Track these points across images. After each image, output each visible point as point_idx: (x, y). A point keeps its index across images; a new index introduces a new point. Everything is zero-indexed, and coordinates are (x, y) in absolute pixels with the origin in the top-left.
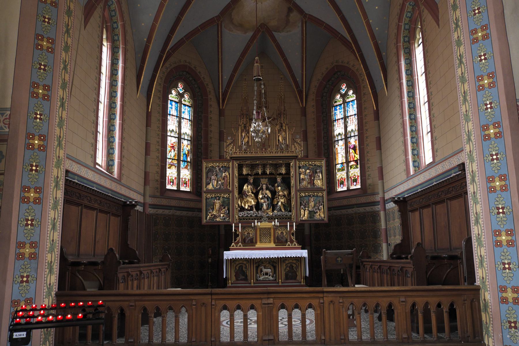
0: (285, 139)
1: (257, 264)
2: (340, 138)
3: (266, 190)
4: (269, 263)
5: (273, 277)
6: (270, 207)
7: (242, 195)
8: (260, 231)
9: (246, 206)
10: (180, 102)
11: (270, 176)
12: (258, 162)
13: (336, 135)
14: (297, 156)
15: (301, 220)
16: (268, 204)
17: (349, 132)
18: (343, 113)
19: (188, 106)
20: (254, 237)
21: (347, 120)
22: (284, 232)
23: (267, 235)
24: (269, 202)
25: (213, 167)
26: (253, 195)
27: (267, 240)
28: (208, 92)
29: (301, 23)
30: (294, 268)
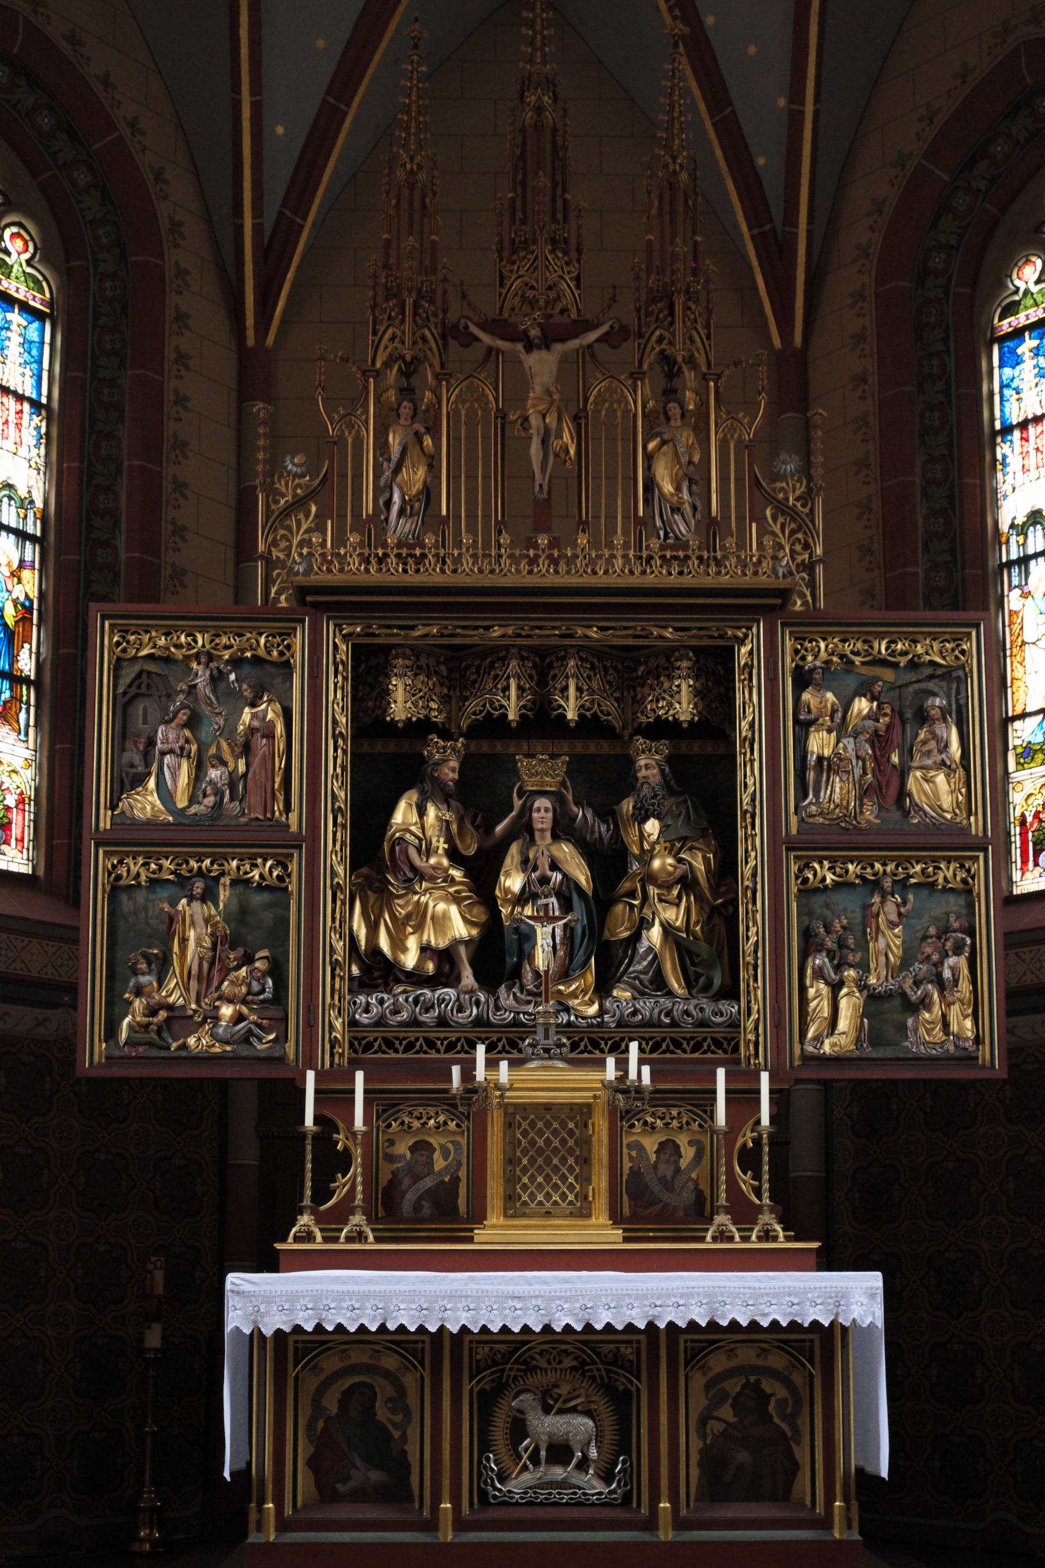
3: (555, 837)
4: (580, 1368)
5: (607, 1477)
6: (580, 957)
7: (381, 869)
8: (509, 1125)
9: (405, 950)
12: (497, 632)
13: (1012, 526)
14: (785, 594)
19: (25, 307)
20: (463, 1174)
22: (682, 1140)
23: (563, 1160)
24: (578, 915)
26: (457, 874)
27: (564, 1196)
30: (771, 1408)
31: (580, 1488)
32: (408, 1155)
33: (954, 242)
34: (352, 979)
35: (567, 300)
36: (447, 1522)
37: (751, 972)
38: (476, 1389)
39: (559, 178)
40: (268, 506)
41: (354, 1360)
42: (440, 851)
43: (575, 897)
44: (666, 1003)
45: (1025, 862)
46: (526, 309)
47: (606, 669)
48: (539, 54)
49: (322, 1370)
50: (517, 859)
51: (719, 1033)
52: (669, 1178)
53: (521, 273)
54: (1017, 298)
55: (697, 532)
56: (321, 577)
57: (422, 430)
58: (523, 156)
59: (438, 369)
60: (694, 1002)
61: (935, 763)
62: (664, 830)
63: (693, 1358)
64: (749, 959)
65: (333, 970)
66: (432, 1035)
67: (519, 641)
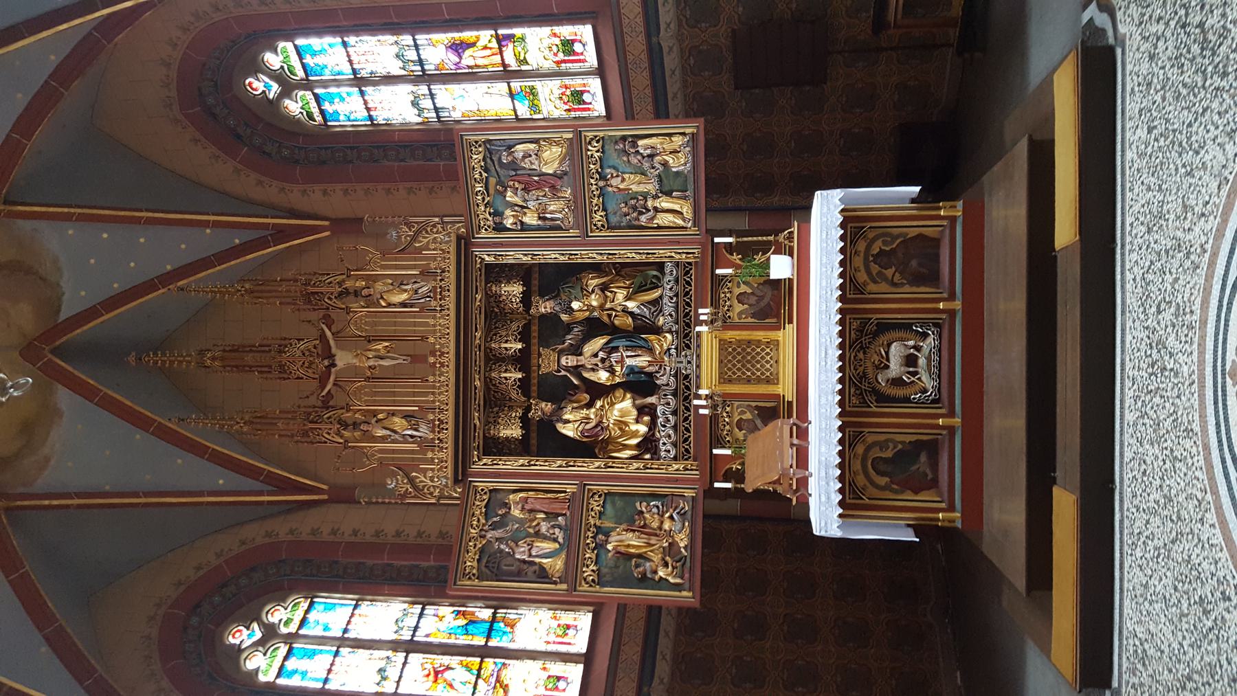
0: (399, 282)
1: (871, 399)
2: (426, 103)
3: (581, 354)
4: (864, 349)
5: (924, 336)
6: (642, 343)
7: (596, 442)
8: (730, 381)
9: (637, 431)
10: (291, 638)
11: (535, 341)
12: (477, 383)
13: (419, 116)
14: (459, 238)
15: (696, 223)
16: (627, 348)
17: (404, 68)
18: (344, 90)
19: (307, 612)
20: (754, 404)
21: (364, 74)
22: (737, 291)
23: (749, 354)
24: (621, 343)
25: (482, 551)
26: (599, 404)
27: (768, 354)
28: (267, 540)
29: (20, 222)
30: (887, 249)
31: (931, 350)
32: (744, 432)
33: (278, 145)
34: (652, 459)
35: (310, 345)
36: (949, 421)
37: (650, 256)
38: (875, 404)
39: (248, 349)
40: (412, 497)
41: (859, 467)
42: (588, 412)
43: (611, 345)
44: (666, 300)
45: (589, 109)
46: (314, 366)
47: (496, 328)
48: (187, 358)
49: (865, 485)
50: (592, 373)
51: (682, 272)
52: (756, 298)
53: (295, 368)
54: (305, 113)
55: (428, 281)
56: (450, 471)
57: (375, 419)
58: (237, 367)
59: (344, 411)
60: (665, 285)
61: (536, 159)
62: (577, 299)
63: (859, 290)
64: (644, 257)
65: (648, 468)
66: (682, 419)
67: (482, 372)
